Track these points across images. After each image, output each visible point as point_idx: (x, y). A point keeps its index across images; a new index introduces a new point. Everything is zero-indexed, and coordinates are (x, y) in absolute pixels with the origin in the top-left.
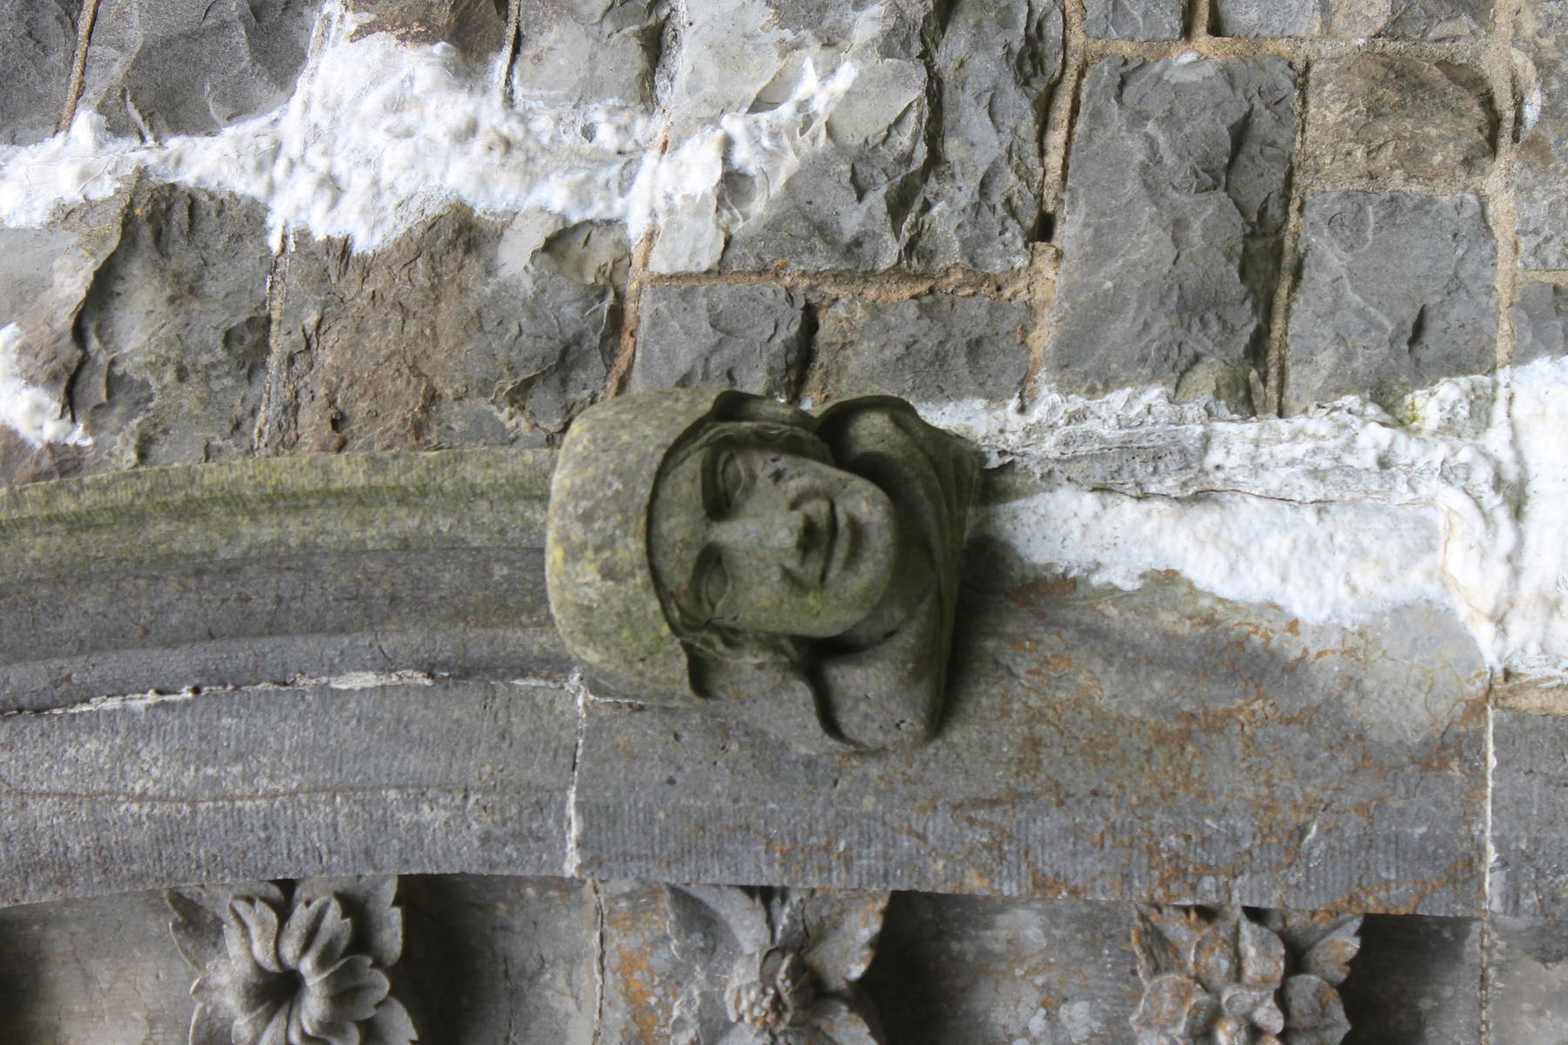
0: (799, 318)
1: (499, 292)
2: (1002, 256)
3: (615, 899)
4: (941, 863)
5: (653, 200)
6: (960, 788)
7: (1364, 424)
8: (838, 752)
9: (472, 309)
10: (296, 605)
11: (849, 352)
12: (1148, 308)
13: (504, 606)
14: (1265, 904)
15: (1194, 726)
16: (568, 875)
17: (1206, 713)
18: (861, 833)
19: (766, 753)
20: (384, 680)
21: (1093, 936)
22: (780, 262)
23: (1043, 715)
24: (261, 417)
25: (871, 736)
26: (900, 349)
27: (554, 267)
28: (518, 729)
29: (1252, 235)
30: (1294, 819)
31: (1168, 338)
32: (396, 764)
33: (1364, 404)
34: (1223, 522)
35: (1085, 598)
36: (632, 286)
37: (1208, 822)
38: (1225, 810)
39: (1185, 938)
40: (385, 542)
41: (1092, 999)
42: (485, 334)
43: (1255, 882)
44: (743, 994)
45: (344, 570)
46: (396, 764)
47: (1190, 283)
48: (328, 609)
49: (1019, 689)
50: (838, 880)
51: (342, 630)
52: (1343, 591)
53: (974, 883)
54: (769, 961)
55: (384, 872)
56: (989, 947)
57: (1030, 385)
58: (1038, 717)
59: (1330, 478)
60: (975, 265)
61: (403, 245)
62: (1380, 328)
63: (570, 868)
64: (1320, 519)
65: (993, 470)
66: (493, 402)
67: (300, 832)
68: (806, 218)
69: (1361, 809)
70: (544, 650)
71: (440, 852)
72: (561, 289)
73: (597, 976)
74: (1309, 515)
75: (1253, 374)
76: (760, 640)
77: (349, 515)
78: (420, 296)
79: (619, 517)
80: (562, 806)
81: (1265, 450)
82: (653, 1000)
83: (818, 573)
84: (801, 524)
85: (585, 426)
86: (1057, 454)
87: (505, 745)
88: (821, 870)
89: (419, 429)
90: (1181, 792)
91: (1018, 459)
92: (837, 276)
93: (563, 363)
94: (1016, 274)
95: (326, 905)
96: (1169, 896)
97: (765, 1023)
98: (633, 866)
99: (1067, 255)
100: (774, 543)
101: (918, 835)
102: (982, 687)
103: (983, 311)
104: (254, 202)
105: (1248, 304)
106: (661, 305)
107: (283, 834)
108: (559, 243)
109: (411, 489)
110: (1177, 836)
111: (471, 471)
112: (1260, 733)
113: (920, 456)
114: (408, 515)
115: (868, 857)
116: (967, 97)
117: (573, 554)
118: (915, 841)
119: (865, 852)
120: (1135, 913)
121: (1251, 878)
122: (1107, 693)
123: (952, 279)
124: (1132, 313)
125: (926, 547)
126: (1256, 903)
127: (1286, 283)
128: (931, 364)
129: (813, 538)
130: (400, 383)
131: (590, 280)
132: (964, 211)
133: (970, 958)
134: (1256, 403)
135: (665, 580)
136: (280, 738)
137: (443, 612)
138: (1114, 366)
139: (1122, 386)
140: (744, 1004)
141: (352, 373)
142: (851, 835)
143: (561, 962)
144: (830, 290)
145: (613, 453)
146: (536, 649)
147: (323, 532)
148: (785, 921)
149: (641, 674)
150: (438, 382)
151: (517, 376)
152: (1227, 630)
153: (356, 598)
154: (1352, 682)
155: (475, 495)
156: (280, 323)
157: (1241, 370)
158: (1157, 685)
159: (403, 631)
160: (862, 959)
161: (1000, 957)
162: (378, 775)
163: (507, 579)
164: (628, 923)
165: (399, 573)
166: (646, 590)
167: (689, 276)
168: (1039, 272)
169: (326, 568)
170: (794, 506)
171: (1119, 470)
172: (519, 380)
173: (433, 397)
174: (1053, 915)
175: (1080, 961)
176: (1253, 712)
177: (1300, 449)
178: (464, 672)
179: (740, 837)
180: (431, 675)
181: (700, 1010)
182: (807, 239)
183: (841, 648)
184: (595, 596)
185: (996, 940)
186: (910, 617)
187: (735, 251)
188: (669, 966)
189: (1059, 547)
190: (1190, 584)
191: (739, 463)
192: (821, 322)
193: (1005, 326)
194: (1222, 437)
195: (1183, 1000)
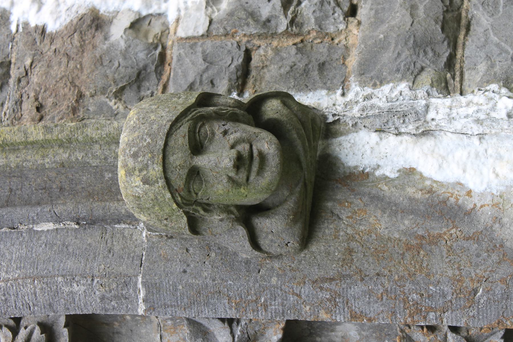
0: (243, 55)
1: (110, 48)
2: (333, 24)
4: (308, 308)
5: (178, 4)
6: (316, 273)
7: (500, 97)
8: (260, 257)
9: (98, 56)
10: (19, 192)
11: (265, 70)
12: (400, 47)
13: (110, 191)
14: (458, 325)
15: (424, 242)
16: (140, 314)
18: (271, 294)
20: (57, 226)
21: (380, 334)
22: (234, 30)
23: (354, 238)
24: (6, 106)
25: (274, 250)
26: (288, 68)
27: (135, 35)
28: (117, 248)
29: (447, 11)
30: (471, 286)
31: (409, 59)
33: (500, 88)
34: (436, 145)
35: (373, 182)
36: (170, 43)
37: (431, 288)
38: (439, 282)
40: (54, 165)
42: (104, 66)
43: (453, 315)
45: (39, 176)
47: (419, 34)
48: (32, 194)
49: (343, 225)
50: (262, 316)
51: (39, 204)
52: (492, 176)
53: (324, 316)
55: (58, 314)
56: (334, 339)
57: (347, 83)
58: (351, 238)
59: (485, 123)
60: (321, 29)
61: (68, 28)
62: (507, 52)
63: (141, 311)
64: (481, 142)
65: (330, 123)
66: (107, 97)
67: (20, 296)
68: (245, 10)
69: (503, 280)
70: (127, 211)
71: (82, 305)
72: (137, 45)
74: (475, 140)
75: (449, 75)
76: (221, 208)
77: (37, 153)
78: (75, 50)
79: (150, 155)
80: (136, 284)
81: (454, 111)
83: (245, 178)
84: (235, 156)
85: (135, 112)
86: (359, 115)
87: (110, 256)
88: (253, 311)
89: (74, 110)
90: (418, 273)
91: (341, 118)
92: (260, 36)
93: (138, 79)
94: (340, 32)
95: (34, 328)
98: (169, 310)
99: (363, 23)
100: (223, 165)
102: (326, 225)
103: (325, 50)
104: (5, 10)
105: (446, 43)
106: (182, 51)
107: (13, 297)
108: (135, 25)
109: (64, 140)
110: (417, 294)
111: (90, 132)
112: (455, 244)
113: (295, 119)
114: (63, 152)
115: (275, 305)
117: (130, 173)
118: (296, 297)
119: (273, 303)
120: (398, 329)
121: (452, 313)
122: (383, 227)
123: (311, 36)
124: (392, 49)
125: (298, 161)
126: (454, 324)
127: (463, 32)
128: (302, 75)
129: (240, 162)
130: (66, 90)
131: (151, 41)
132: (316, 4)
134: (450, 88)
136: (11, 253)
137: (83, 194)
138: (385, 73)
139: (388, 83)
141: (46, 86)
142: (267, 295)
144: (257, 42)
145: (147, 125)
146: (123, 211)
147: (26, 160)
148: (239, 333)
150: (83, 89)
151: (117, 85)
152: (438, 195)
153: (45, 189)
154: (497, 220)
155: (93, 142)
156: (15, 64)
157: (443, 74)
158: (406, 222)
159: (64, 204)
164: (172, 330)
165: (63, 177)
166: (164, 189)
167: (194, 38)
168: (350, 31)
169: (31, 176)
170: (232, 147)
171: (387, 122)
172: (119, 87)
173: (81, 96)
176: (451, 235)
177: (471, 110)
178: (93, 222)
180: (78, 224)
182: (246, 20)
183: (261, 209)
184: (140, 192)
185: (337, 337)
186: (291, 194)
187: (214, 26)
189: (360, 158)
190: (421, 174)
191: (207, 127)
192: (253, 57)
193: (336, 56)
194: (435, 106)
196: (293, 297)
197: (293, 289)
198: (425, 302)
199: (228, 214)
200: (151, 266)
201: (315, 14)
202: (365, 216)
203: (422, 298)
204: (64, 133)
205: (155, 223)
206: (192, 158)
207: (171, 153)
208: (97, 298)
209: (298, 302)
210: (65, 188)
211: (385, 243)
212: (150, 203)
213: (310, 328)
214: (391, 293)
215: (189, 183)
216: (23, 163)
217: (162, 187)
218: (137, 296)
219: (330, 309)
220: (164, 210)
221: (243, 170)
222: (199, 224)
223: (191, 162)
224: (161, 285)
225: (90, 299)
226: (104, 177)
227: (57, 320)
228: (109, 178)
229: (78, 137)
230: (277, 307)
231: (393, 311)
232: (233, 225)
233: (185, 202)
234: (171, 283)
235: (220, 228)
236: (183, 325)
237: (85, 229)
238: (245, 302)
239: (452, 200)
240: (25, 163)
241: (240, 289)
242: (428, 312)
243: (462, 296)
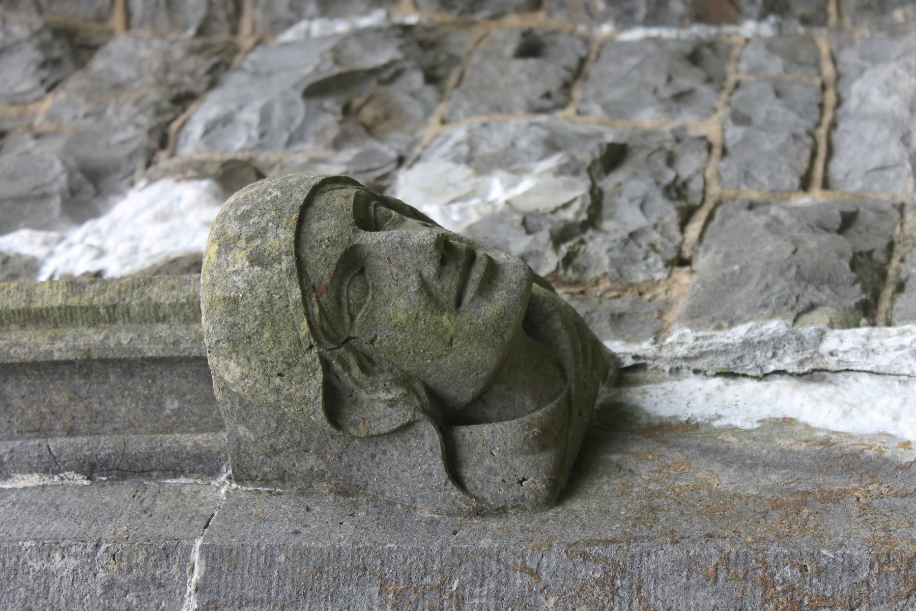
4: (552, 600)
6: (575, 534)
18: (475, 571)
20: (47, 480)
37: (824, 552)
46: (39, 527)
70: (196, 445)
71: (63, 600)
79: (273, 213)
80: (188, 551)
91: (649, 362)
101: (532, 573)
110: (792, 567)
115: (480, 596)
116: (622, 201)
118: (528, 578)
135: (310, 273)
139: (745, 322)
142: (465, 574)
147: (18, 344)
149: (277, 390)
179: (355, 577)
184: (241, 285)
196: (522, 578)
197: (524, 557)
198: (811, 585)
201: (611, 254)
202: (687, 470)
203: (803, 576)
204: (106, 295)
205: (256, 381)
206: (354, 231)
207: (316, 217)
208: (98, 586)
209: (531, 590)
214: (736, 564)
215: (341, 283)
216: (11, 348)
217: (287, 270)
218: (186, 579)
219: (600, 604)
220: (280, 343)
221: (454, 270)
223: (352, 237)
224: (242, 554)
225: (81, 588)
228: (172, 410)
229: (130, 302)
230: (484, 600)
233: (325, 325)
234: (263, 548)
238: (416, 591)
239: (871, 453)
240: (14, 349)
241: (409, 561)
243: (892, 569)
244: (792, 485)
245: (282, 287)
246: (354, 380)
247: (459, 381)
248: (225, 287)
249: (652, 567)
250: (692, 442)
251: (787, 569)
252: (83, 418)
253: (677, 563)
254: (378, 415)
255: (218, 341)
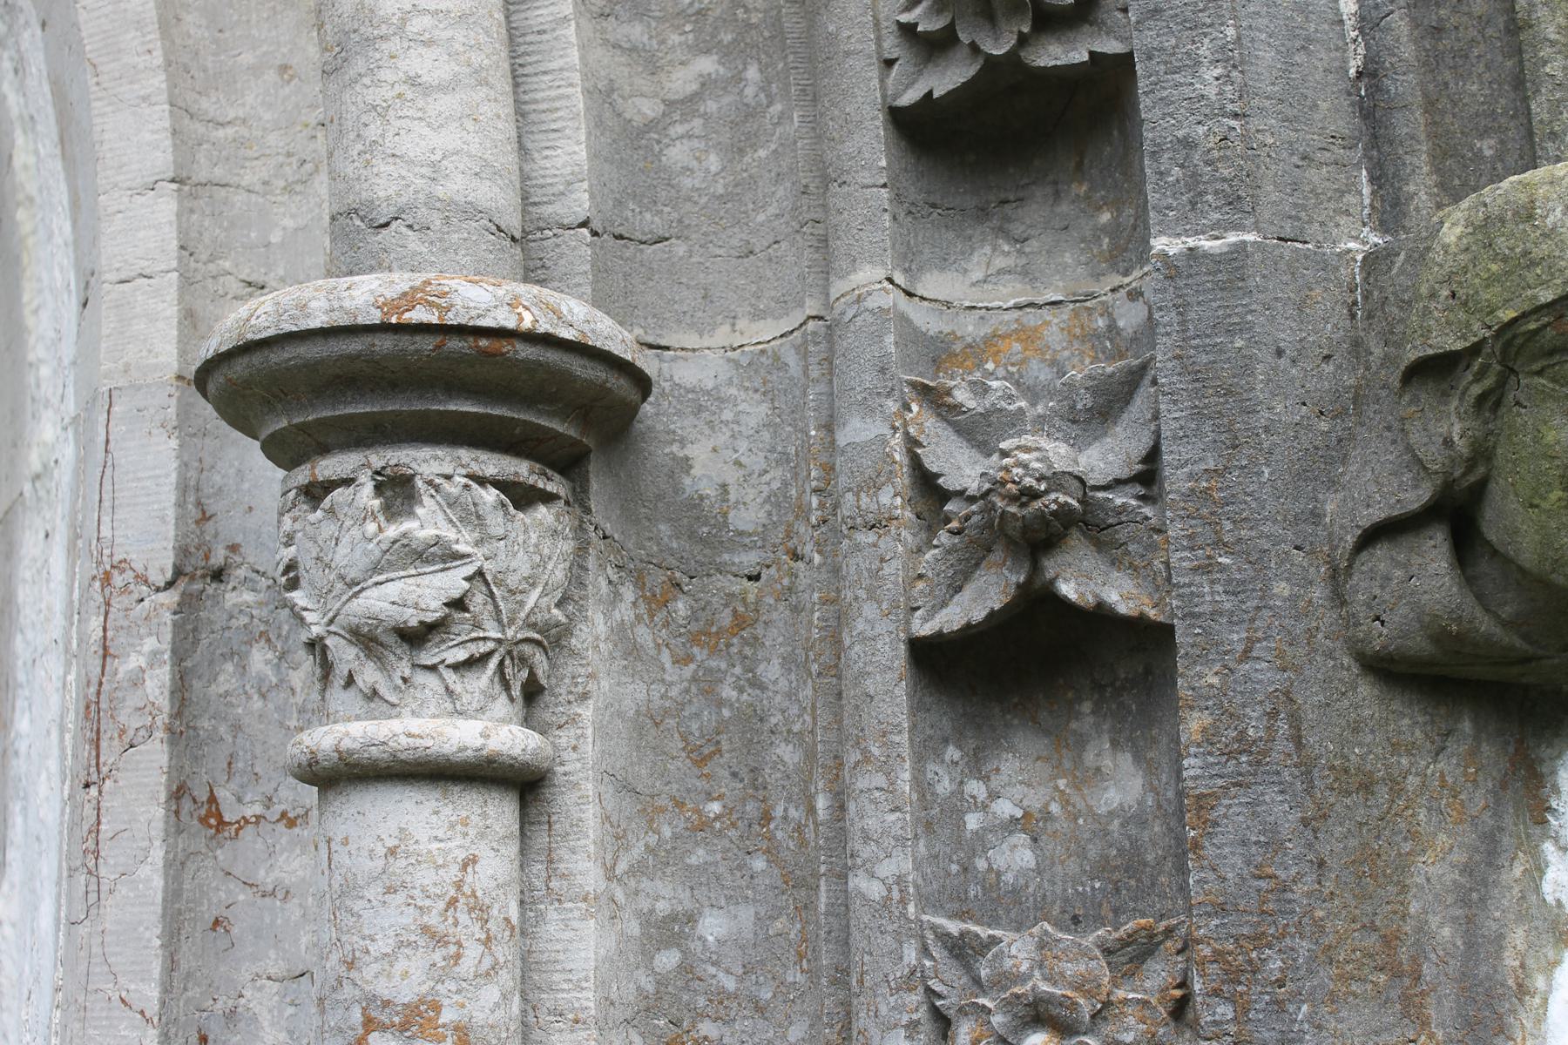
3: (1107, 311)
4: (1215, 680)
6: (1310, 699)
15: (1407, 981)
16: (1153, 242)
17: (1423, 994)
19: (1323, 465)
21: (1116, 867)
25: (1361, 586)
28: (1314, 175)
32: (1263, 36)
35: (1528, 836)
37: (1305, 1008)
38: (1319, 1027)
39: (1148, 984)
41: (1039, 871)
44: (1036, 454)
46: (1263, 36)
53: (1194, 724)
54: (1076, 484)
58: (1396, 786)
63: (1160, 243)
70: (1412, 196)
71: (1165, 93)
73: (1011, 303)
82: (990, 366)
87: (1295, 159)
88: (1190, 537)
96: (1202, 962)
97: (1003, 483)
101: (1247, 651)
110: (1281, 970)
115: (1212, 593)
118: (1240, 648)
133: (1074, 725)
137: (1431, 87)
140: (1024, 457)
142: (1239, 570)
143: (1023, 261)
146: (1412, 188)
148: (1119, 501)
149: (1433, 295)
152: (1515, 1012)
160: (1082, 595)
161: (1078, 761)
162: (1249, 16)
163: (1478, 155)
164: (1078, 331)
174: (1140, 820)
175: (1082, 854)
180: (1360, 74)
181: (1001, 410)
184: (1550, 221)
188: (1031, 382)
190: (1557, 963)
195: (1078, 988)
199: (1469, 460)
200: (1282, 266)
203: (1272, 983)
205: (1441, 266)
210: (1440, 39)
211: (1395, 878)
212: (1512, 249)
213: (1118, 684)
218: (1203, 233)
219: (1215, 739)
220: (1487, 286)
222: (1431, 385)
224: (1240, 293)
226: (1481, 137)
227: (1108, 34)
228: (1480, 149)
230: (1208, 598)
231: (1228, 907)
232: (1436, 473)
233: (1519, 341)
234: (1249, 318)
235: (1426, 440)
236: (1095, 359)
237: (1349, 94)
242: (1235, 1002)
244: (1433, 956)
245: (1552, 275)
246: (1467, 389)
247: (1512, 521)
248: (1548, 199)
249: (1267, 798)
250: (1508, 821)
251: (1279, 963)
252: (1458, 40)
253: (1274, 829)
254: (1431, 427)
255: (1485, 205)
